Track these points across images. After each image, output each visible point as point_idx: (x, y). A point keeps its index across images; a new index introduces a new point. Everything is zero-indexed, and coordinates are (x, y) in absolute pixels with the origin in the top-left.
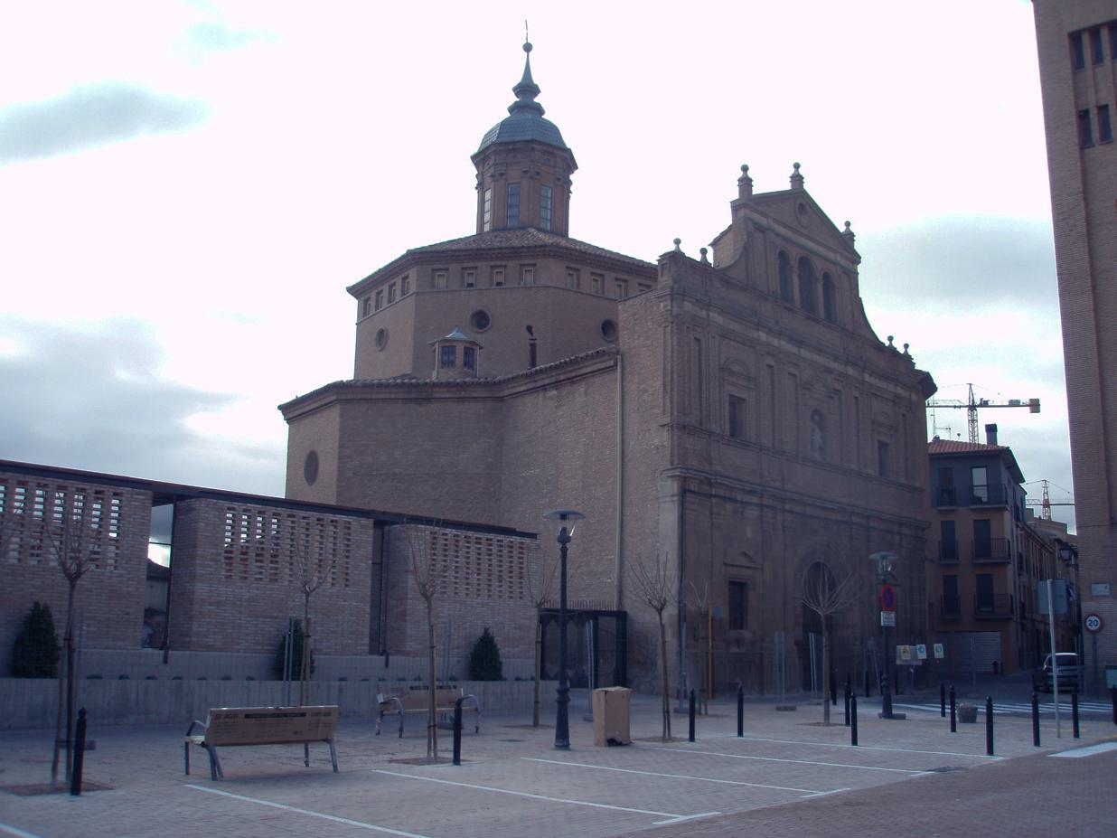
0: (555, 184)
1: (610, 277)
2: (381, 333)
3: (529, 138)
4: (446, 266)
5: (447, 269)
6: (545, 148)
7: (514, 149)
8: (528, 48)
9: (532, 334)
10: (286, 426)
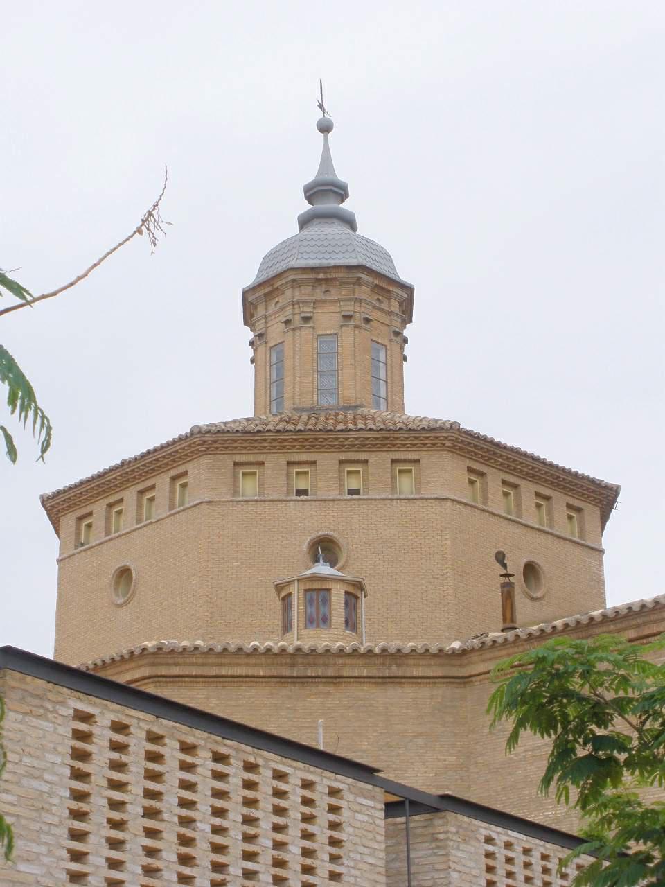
1: (528, 489)
2: (124, 574)
3: (353, 262)
4: (261, 458)
5: (262, 463)
6: (376, 282)
7: (326, 280)
8: (325, 128)
9: (505, 566)
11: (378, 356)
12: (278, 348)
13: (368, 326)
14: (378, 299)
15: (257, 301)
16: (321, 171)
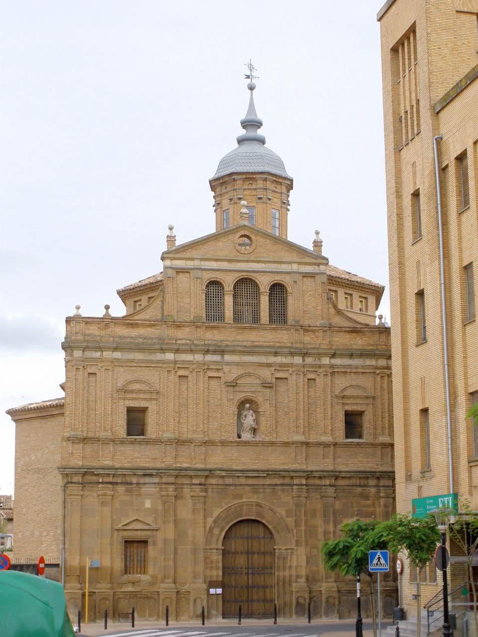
0: (257, 203)
3: (228, 172)
6: (244, 176)
8: (251, 88)
10: (13, 424)
11: (275, 224)
12: (227, 211)
13: (270, 202)
14: (250, 183)
15: (216, 184)
16: (248, 113)
